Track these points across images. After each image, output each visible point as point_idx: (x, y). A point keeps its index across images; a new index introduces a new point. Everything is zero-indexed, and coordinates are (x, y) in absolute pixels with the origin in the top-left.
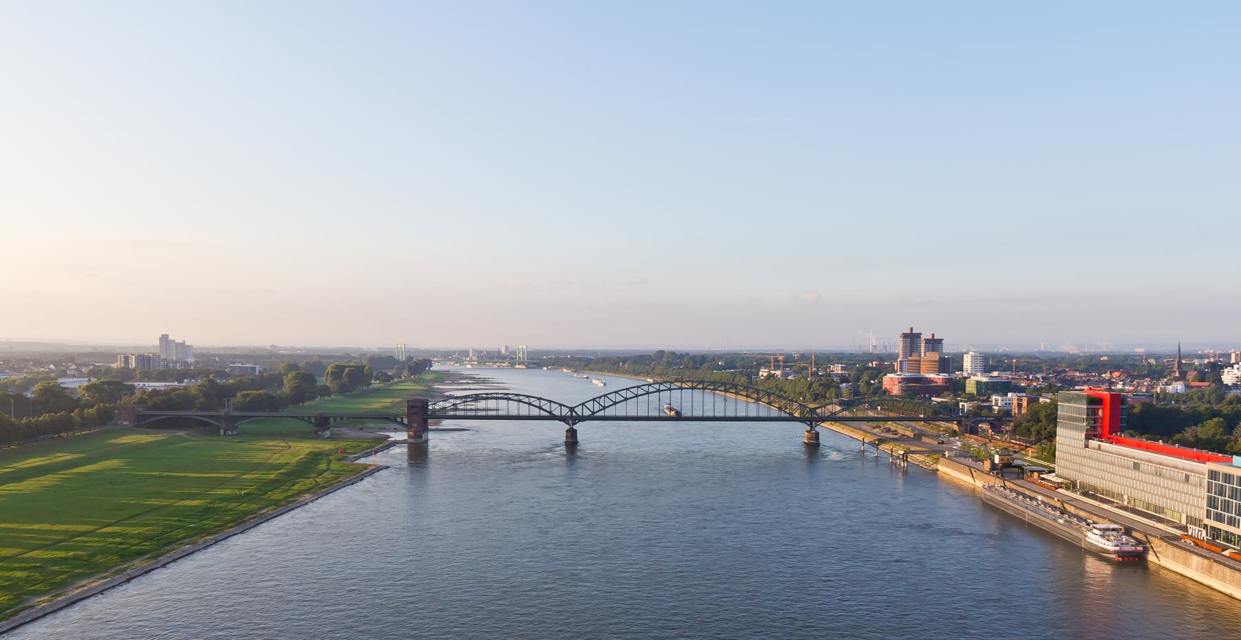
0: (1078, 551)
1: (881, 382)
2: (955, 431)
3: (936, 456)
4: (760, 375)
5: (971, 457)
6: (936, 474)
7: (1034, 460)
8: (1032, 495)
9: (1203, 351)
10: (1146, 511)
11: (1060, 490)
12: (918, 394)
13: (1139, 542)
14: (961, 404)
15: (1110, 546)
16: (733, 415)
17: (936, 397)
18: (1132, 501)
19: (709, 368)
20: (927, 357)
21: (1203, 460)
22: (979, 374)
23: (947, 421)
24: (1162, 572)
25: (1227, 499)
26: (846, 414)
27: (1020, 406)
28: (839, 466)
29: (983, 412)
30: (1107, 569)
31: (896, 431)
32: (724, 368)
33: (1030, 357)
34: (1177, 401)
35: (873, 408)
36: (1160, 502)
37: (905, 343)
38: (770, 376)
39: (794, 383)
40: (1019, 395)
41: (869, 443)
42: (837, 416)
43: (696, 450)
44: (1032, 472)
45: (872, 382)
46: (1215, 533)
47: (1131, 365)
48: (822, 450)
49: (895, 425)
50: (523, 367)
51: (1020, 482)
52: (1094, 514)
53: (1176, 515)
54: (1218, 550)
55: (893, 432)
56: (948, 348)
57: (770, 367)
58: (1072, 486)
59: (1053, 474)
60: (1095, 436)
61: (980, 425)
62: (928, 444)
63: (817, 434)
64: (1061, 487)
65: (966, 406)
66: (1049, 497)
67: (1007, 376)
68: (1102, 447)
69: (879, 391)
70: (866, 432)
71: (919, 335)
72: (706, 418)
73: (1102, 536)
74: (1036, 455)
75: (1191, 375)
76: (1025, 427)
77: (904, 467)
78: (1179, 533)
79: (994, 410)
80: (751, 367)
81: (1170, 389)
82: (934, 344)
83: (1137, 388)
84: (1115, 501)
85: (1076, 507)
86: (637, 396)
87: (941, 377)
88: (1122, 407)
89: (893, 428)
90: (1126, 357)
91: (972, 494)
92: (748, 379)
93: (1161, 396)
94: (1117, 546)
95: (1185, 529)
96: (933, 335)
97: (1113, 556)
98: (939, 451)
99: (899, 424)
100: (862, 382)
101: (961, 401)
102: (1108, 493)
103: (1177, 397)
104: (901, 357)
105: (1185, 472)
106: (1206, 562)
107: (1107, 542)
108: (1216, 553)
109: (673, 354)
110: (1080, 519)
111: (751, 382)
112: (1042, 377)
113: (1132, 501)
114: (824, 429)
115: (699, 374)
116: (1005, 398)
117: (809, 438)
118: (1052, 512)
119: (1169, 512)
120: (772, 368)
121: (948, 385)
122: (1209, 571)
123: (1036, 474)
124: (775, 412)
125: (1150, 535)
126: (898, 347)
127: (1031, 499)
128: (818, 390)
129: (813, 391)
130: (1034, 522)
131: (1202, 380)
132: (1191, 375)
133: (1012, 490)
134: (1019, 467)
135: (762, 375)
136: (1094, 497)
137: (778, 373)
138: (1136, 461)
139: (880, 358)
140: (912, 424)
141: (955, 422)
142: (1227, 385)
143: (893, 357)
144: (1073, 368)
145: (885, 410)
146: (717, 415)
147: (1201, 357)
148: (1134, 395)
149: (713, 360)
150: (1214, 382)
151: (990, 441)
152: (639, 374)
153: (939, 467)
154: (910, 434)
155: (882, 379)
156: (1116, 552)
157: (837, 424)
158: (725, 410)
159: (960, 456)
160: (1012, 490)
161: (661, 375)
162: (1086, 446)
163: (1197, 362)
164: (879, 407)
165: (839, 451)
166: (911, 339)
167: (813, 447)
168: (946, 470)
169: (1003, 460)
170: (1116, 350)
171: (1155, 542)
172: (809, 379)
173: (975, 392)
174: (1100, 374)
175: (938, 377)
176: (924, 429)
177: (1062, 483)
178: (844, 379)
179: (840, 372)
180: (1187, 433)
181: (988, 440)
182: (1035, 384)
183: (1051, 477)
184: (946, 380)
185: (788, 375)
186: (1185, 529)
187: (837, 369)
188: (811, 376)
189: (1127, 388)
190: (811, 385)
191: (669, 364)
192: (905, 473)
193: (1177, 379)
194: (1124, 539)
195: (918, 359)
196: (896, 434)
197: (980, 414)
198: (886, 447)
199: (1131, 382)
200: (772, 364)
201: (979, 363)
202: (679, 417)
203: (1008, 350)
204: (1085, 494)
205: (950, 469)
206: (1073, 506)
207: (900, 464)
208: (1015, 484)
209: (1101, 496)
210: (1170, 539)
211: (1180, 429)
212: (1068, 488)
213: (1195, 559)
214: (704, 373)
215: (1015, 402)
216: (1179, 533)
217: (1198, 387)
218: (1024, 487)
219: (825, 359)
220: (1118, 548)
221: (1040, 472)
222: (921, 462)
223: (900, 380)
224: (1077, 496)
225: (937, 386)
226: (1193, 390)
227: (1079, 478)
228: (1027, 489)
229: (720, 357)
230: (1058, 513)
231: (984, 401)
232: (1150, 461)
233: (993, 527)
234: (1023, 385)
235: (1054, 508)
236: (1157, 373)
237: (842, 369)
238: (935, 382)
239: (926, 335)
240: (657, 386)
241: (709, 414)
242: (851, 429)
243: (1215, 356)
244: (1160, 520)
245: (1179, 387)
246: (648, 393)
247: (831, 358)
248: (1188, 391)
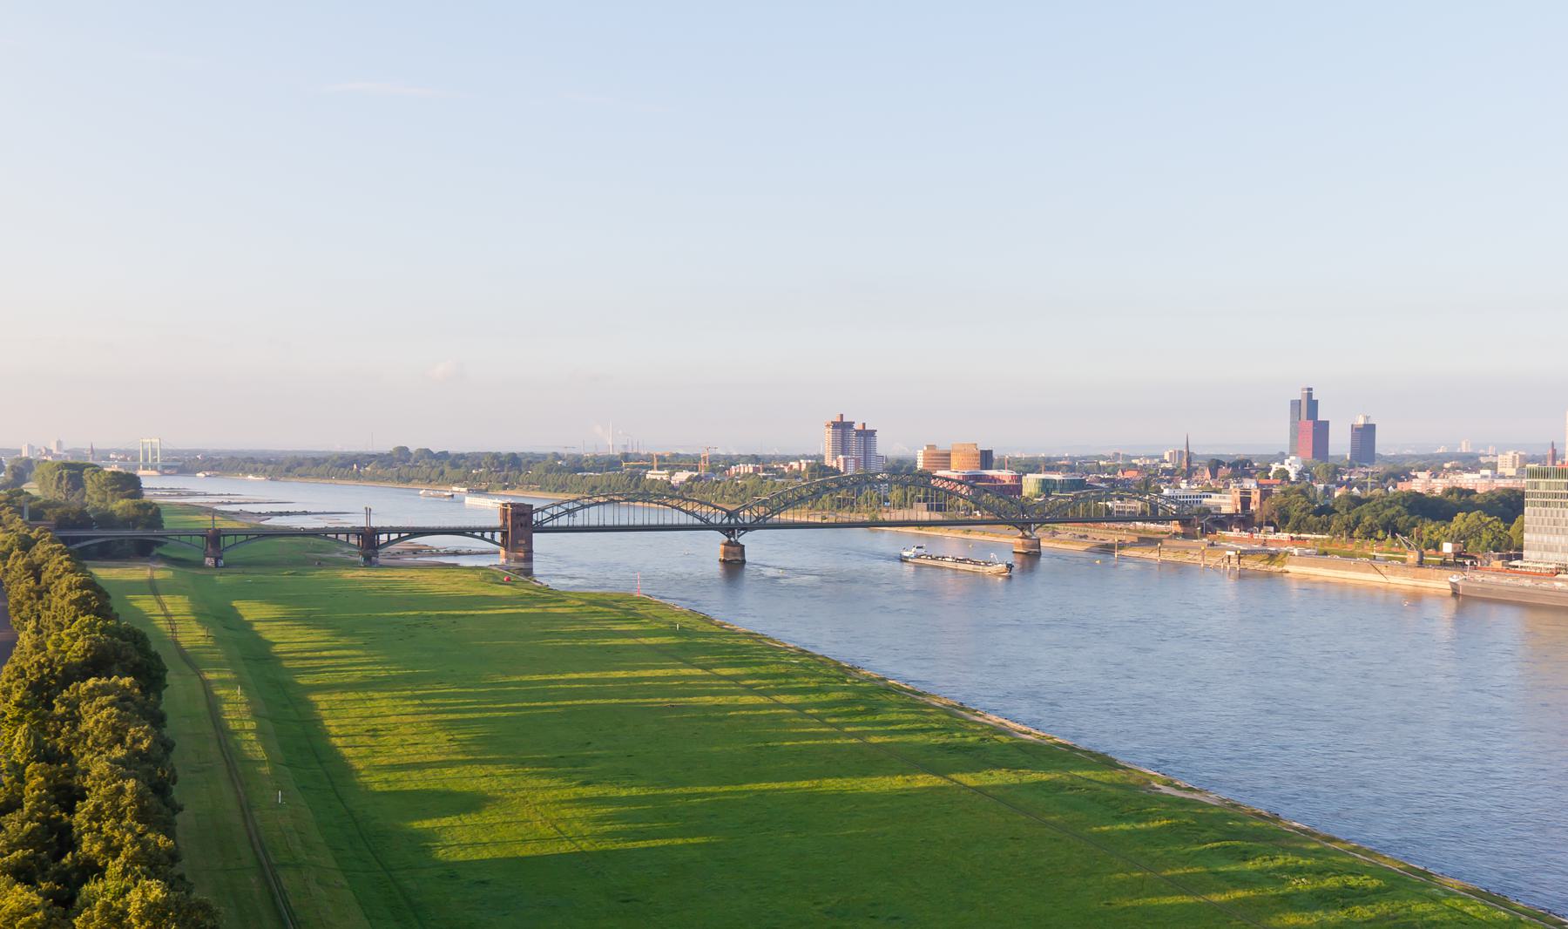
37: (834, 434)
42: (544, 525)
50: (154, 473)
71: (850, 425)
96: (864, 424)
238: (1000, 481)
239: (858, 426)
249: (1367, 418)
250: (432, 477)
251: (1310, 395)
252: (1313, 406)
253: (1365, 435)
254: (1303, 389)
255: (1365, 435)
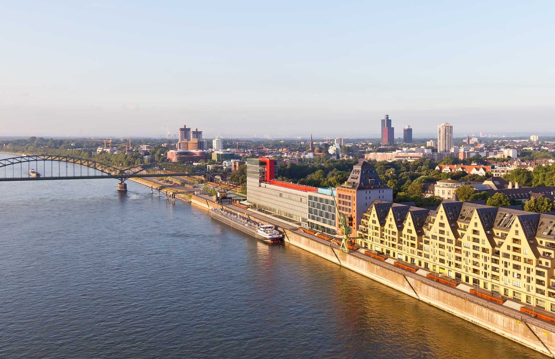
0: (253, 240)
1: (166, 154)
2: (203, 180)
3: (190, 194)
4: (97, 151)
5: (208, 194)
6: (190, 204)
7: (240, 194)
8: (235, 212)
9: (325, 138)
10: (286, 217)
11: (249, 209)
12: (186, 161)
13: (281, 233)
14: (208, 166)
15: (268, 236)
16: (58, 176)
17: (195, 162)
18: (280, 212)
19: (65, 147)
20: (193, 140)
21: (306, 190)
22: (220, 150)
23: (200, 175)
24: (291, 247)
25: (316, 209)
26: (144, 172)
27: (235, 166)
28: (136, 202)
29: (218, 170)
30: (267, 247)
31: (172, 181)
32: (75, 147)
33: (248, 141)
34: (310, 162)
35: (161, 169)
36: (291, 212)
37: (182, 133)
38: (103, 152)
39: (117, 156)
40: (234, 160)
41: (156, 189)
43: (46, 197)
44: (236, 200)
45: (162, 155)
46: (312, 225)
47: (293, 145)
48: (129, 194)
49: (171, 178)
51: (230, 206)
52: (262, 220)
53: (298, 218)
54: (313, 233)
55: (170, 182)
56: (204, 136)
57: (104, 147)
58: (254, 206)
59: (246, 201)
60: (263, 181)
61: (216, 177)
62: (187, 188)
63: (125, 185)
64: (249, 207)
65: (210, 167)
66: (243, 213)
67: (234, 150)
68: (267, 186)
69: (165, 160)
70: (155, 183)
71: (189, 129)
72: (76, 177)
73: (264, 231)
74: (241, 191)
75: (317, 149)
76: (237, 177)
77: (173, 201)
78: (298, 226)
79: (224, 168)
80: (92, 147)
81: (307, 156)
82: (197, 134)
83: (293, 156)
84: (272, 212)
85: (255, 217)
86: (13, 163)
87: (198, 152)
88: (275, 166)
89: (170, 180)
90: (292, 141)
91: (208, 214)
92: (88, 154)
93: (303, 160)
94: (271, 235)
95: (300, 224)
97: (269, 241)
98: (192, 192)
99: (174, 178)
100: (156, 155)
101: (208, 164)
102: (270, 209)
103: (310, 160)
104: (180, 141)
105: (300, 197)
106: (307, 240)
107: (266, 234)
108: (312, 235)
109: (42, 139)
110: (255, 223)
111: (90, 156)
112: (251, 151)
113: (280, 212)
114: (131, 183)
115: (58, 151)
116: (229, 162)
117: (120, 187)
118: (243, 221)
119: (295, 217)
120: (105, 147)
121: (202, 156)
122: (308, 244)
123: (238, 201)
124: (99, 174)
125: (286, 229)
126: (178, 135)
127: (235, 214)
128: (130, 159)
129: (128, 160)
130: (235, 226)
131: (320, 152)
132: (317, 149)
133: (226, 210)
134: (230, 198)
135: (98, 152)
136: (263, 211)
137: (108, 150)
138: (281, 192)
139: (170, 142)
140: (181, 177)
141: (203, 176)
142: (330, 154)
143: (177, 141)
144: (267, 146)
145: (168, 170)
146: (76, 175)
147: (323, 141)
148: (290, 160)
149: (68, 142)
150: (325, 153)
151: (220, 185)
152: (17, 151)
153: (192, 200)
154: (179, 183)
155: (167, 153)
156: (270, 239)
157: (140, 179)
158: (74, 173)
159: (203, 194)
160: (226, 210)
161: (32, 152)
162: (260, 186)
163: (321, 143)
164: (164, 169)
165: (138, 194)
166: (185, 131)
167: (123, 192)
168: (196, 202)
169: (221, 195)
170: (289, 137)
171: (288, 232)
172: (126, 153)
173: (217, 160)
174: (278, 150)
175: (197, 152)
176: (187, 180)
177: (249, 205)
178: (146, 153)
179: (146, 149)
180: (308, 177)
181: (219, 185)
182: (247, 155)
183: (245, 203)
184: (201, 153)
185: (114, 151)
186: (300, 224)
187: (144, 148)
188: (128, 151)
189: (289, 156)
190: (126, 156)
191: (38, 145)
192: (174, 204)
193: (310, 152)
194: (274, 232)
195: (187, 142)
196: (172, 183)
197: (215, 171)
198: (164, 190)
199: (291, 153)
200: (105, 145)
201: (221, 144)
202: (38, 178)
203: (239, 137)
204: (260, 210)
205: (197, 201)
206: (253, 217)
207: (171, 200)
208: (228, 207)
209: (267, 211)
210: (294, 230)
211: (305, 176)
212: (252, 208)
213: (303, 239)
214: (61, 151)
215: (233, 164)
216: (298, 226)
217: (319, 155)
218: (231, 209)
219: (136, 143)
220: (271, 237)
221: (240, 200)
222: (183, 198)
223: (177, 154)
224: (256, 211)
225: (197, 157)
226: (317, 156)
227: (258, 203)
228: (233, 209)
229: (73, 141)
230: (246, 221)
231: (219, 164)
232: (286, 192)
233: (218, 231)
234: (241, 155)
235: (244, 218)
236: (302, 149)
237: (147, 147)
238: (195, 154)
239: (193, 129)
240: (27, 158)
241: (64, 175)
242: (147, 181)
243: (328, 140)
244: (290, 221)
245: (310, 155)
246: (13, 163)
247: (142, 141)
248: (315, 157)
249: (409, 126)
250: (24, 150)
251: (387, 118)
252: (389, 122)
253: (408, 132)
254: (385, 116)
255: (408, 132)
